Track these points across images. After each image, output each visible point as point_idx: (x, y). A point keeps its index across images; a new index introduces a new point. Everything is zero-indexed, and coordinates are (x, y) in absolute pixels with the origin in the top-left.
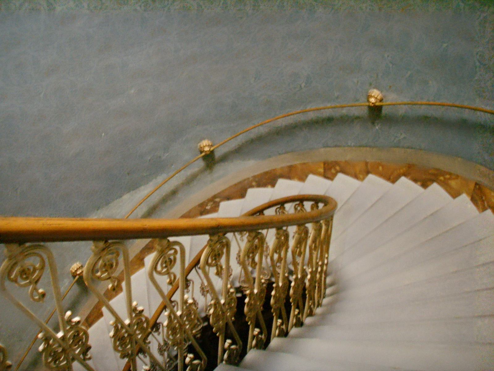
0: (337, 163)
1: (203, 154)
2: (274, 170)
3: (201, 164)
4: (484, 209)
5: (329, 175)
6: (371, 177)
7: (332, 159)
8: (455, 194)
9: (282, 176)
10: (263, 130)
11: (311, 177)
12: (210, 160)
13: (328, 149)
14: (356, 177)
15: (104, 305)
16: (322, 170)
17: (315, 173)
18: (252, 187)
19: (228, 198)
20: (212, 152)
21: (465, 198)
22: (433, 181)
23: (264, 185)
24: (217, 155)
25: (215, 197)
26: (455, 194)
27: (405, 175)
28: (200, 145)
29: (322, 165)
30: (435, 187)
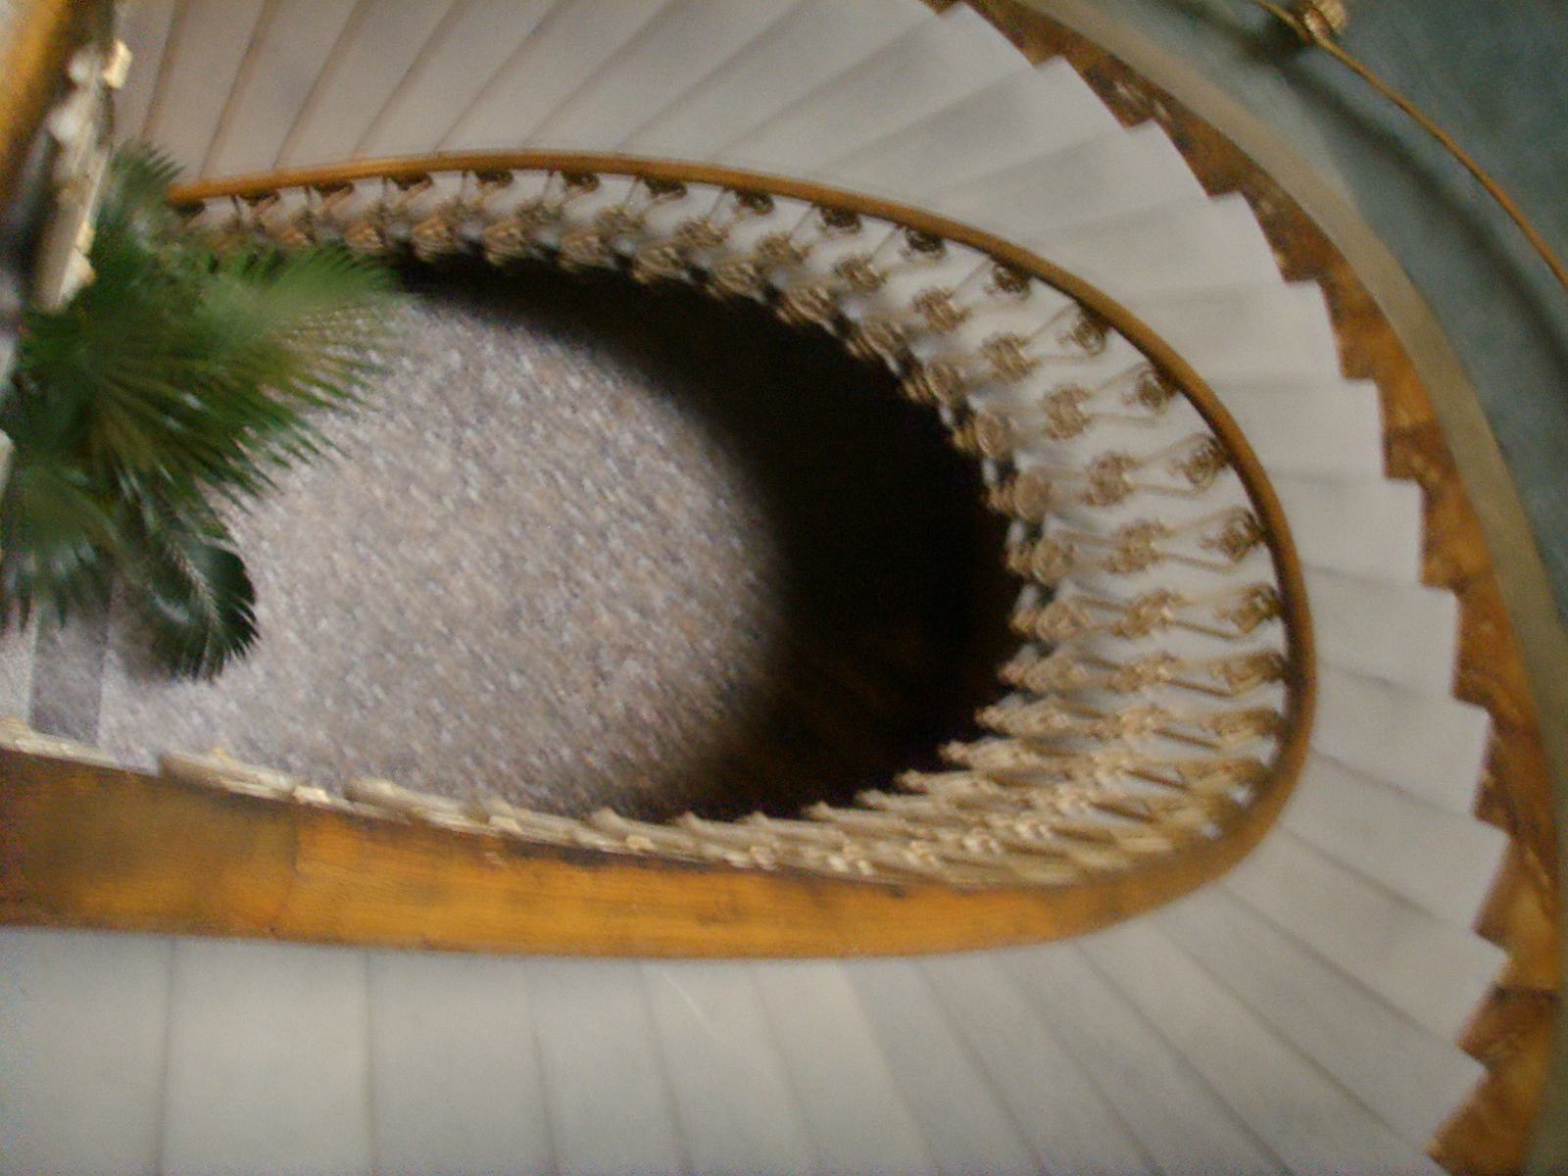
0: (1449, 469)
1: (1289, 19)
2: (1340, 260)
3: (1254, 19)
4: (1475, 1047)
5: (1396, 449)
6: (1447, 607)
7: (1460, 448)
8: (1493, 927)
9: (1332, 292)
10: (1461, 184)
11: (1368, 394)
12: (1280, 47)
13: (1484, 426)
14: (1431, 546)
15: (45, 318)
16: (1405, 420)
17: (1389, 403)
18: (1254, 203)
19: (1183, 144)
20: (1310, 42)
21: (1491, 963)
22: (1513, 828)
23: (1277, 241)
24: (1311, 62)
25: (1167, 99)
26: (1493, 927)
27: (1501, 724)
28: (949, 801)
29: (1422, 417)
30: (1493, 844)
